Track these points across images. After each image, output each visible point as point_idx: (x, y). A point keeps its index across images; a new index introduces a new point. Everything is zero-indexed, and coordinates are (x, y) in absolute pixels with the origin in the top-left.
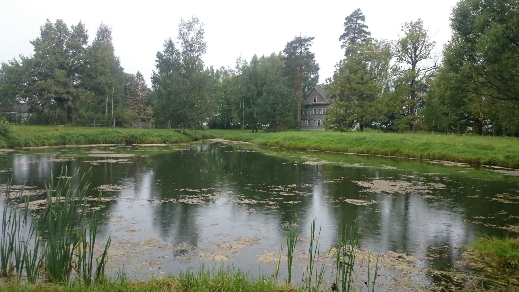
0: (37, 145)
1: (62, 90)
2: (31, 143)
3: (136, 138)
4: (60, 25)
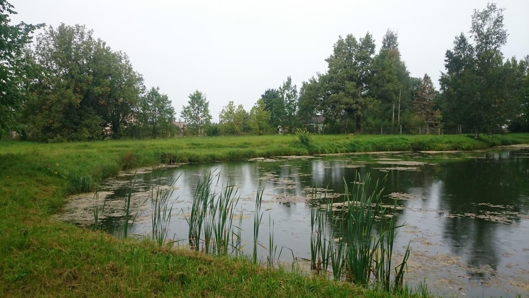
0: (331, 153)
1: (352, 101)
2: (326, 151)
3: (424, 145)
4: (351, 39)
